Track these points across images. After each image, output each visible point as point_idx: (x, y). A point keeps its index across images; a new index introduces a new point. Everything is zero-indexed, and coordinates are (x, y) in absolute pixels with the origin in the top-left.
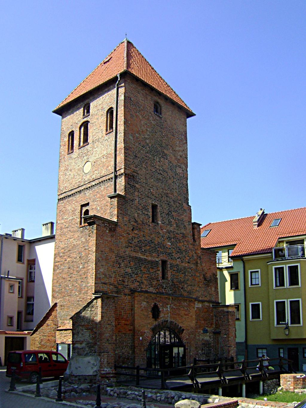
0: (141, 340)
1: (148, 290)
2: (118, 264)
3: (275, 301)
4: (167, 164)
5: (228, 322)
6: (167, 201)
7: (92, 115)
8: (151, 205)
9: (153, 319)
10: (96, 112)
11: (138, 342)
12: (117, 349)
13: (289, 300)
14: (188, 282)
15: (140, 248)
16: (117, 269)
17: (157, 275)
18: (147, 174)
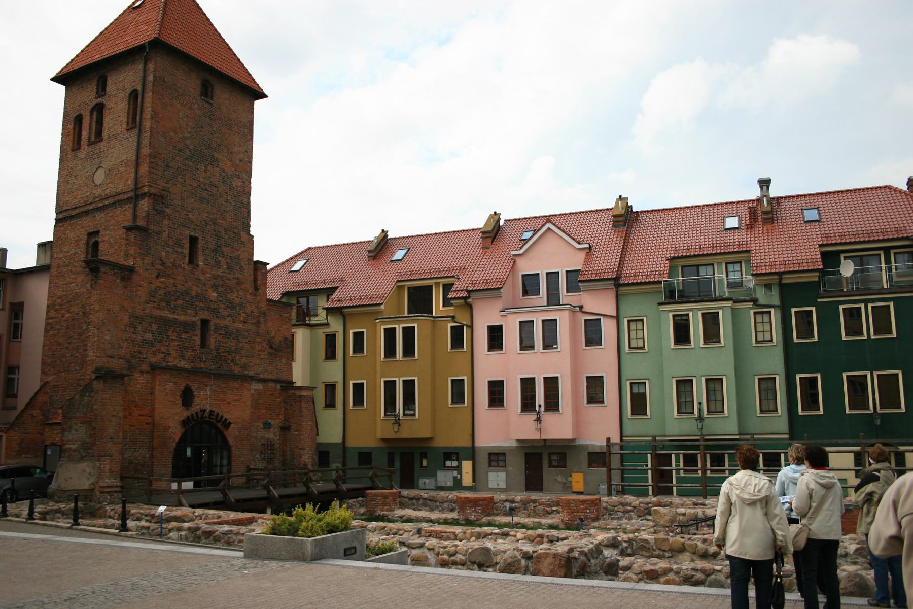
1: (178, 365)
2: (133, 327)
3: (383, 380)
4: (218, 175)
5: (301, 412)
6: (215, 231)
7: (109, 97)
8: (188, 237)
9: (183, 407)
10: (115, 92)
13: (402, 379)
14: (242, 351)
15: (168, 303)
17: (192, 342)
18: (185, 191)
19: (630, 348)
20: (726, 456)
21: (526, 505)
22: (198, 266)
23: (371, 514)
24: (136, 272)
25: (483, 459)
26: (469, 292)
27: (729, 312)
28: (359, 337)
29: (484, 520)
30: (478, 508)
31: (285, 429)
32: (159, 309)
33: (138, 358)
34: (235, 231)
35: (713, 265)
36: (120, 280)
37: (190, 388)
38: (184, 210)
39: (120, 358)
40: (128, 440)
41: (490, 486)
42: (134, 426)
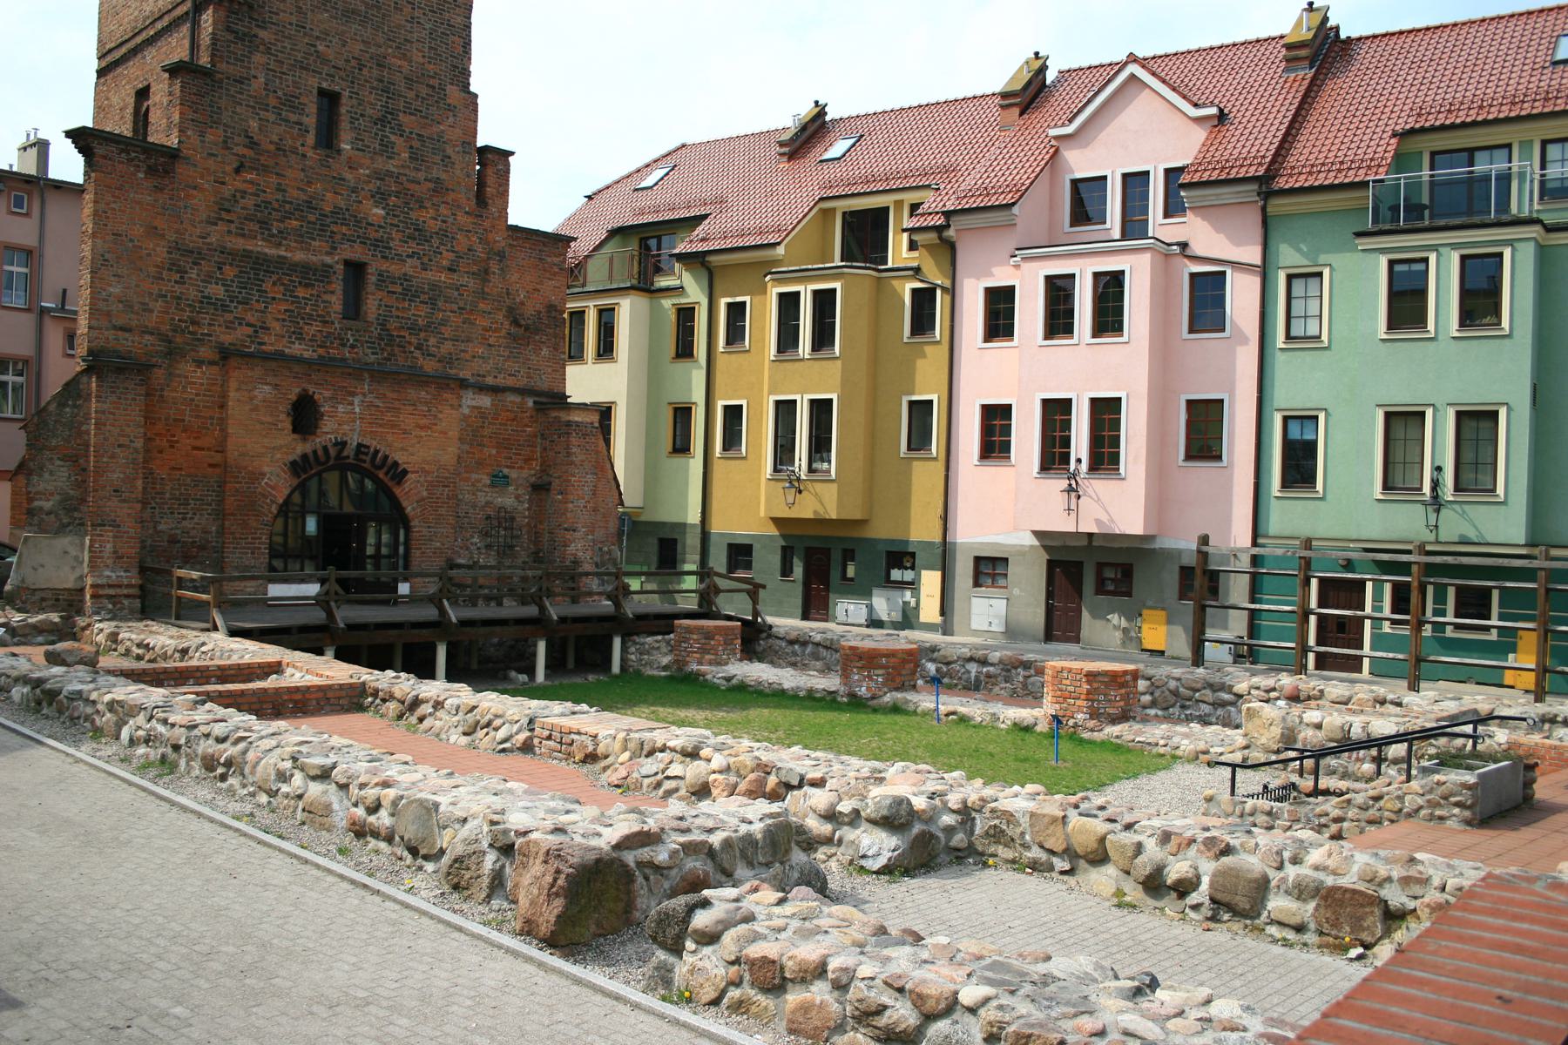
1: (287, 351)
2: (178, 272)
5: (569, 454)
6: (381, 81)
9: (295, 436)
14: (443, 329)
15: (264, 224)
19: (1288, 337)
20: (1495, 594)
21: (1009, 671)
22: (339, 151)
23: (680, 669)
24: (185, 158)
25: (963, 570)
26: (948, 214)
27: (1528, 252)
28: (737, 311)
29: (888, 698)
30: (877, 672)
31: (540, 488)
32: (243, 235)
33: (189, 332)
34: (431, 82)
35: (1509, 146)
36: (146, 173)
37: (312, 397)
38: (305, 34)
39: (146, 331)
40: (168, 495)
41: (974, 626)
42: (181, 469)
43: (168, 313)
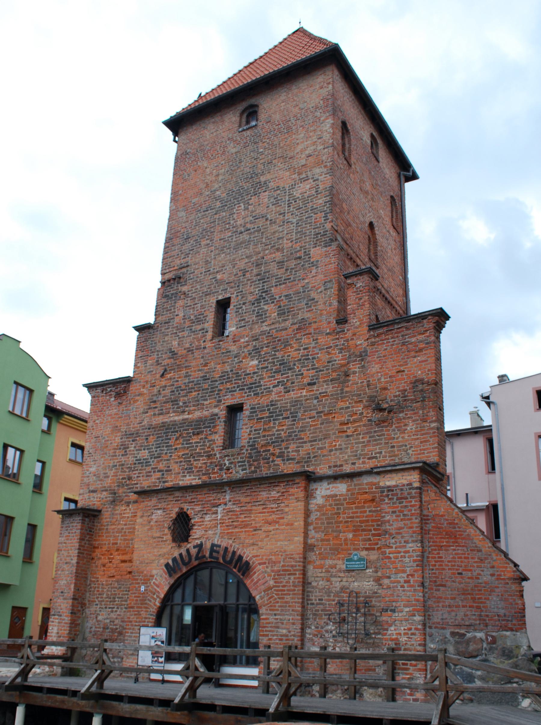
0: (144, 593)
11: (135, 597)
12: (102, 612)
15: (175, 402)
16: (121, 459)
33: (127, 485)
40: (105, 596)
43: (117, 476)
